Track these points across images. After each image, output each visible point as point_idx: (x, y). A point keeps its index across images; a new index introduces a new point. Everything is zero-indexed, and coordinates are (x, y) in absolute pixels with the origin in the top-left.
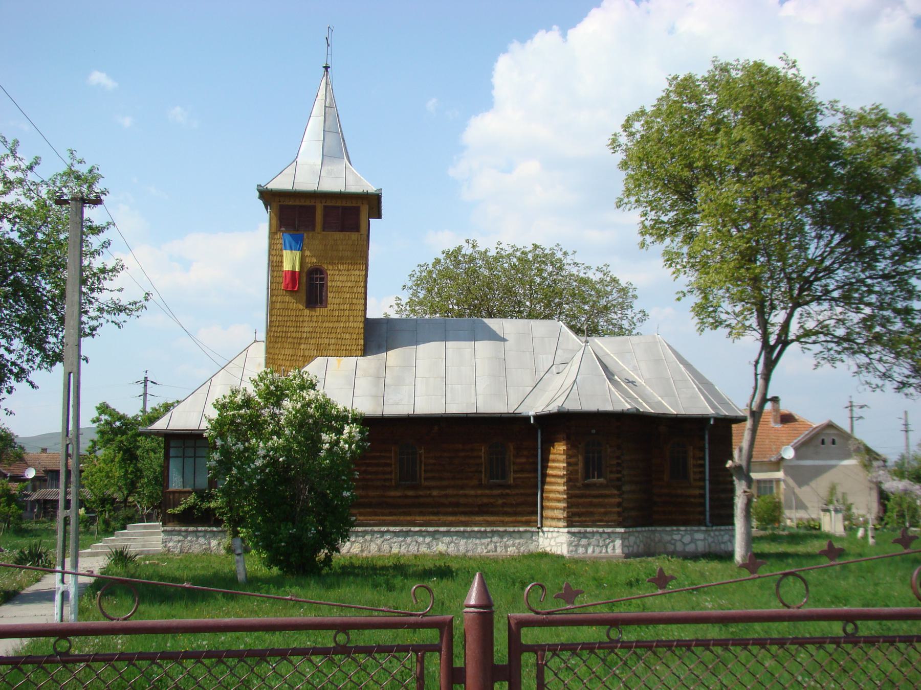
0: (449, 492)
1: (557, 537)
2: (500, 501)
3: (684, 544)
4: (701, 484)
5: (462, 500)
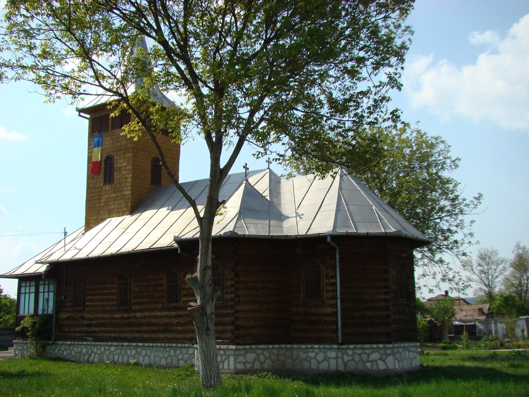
0: (147, 314)
1: (371, 353)
2: (175, 321)
3: (319, 362)
4: (334, 302)
5: (153, 321)
